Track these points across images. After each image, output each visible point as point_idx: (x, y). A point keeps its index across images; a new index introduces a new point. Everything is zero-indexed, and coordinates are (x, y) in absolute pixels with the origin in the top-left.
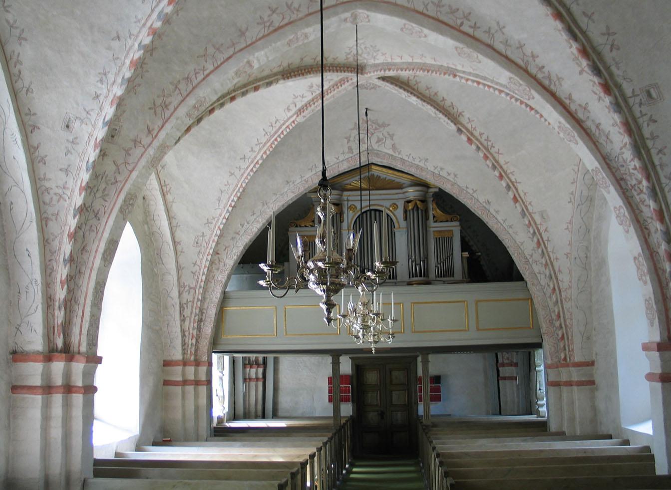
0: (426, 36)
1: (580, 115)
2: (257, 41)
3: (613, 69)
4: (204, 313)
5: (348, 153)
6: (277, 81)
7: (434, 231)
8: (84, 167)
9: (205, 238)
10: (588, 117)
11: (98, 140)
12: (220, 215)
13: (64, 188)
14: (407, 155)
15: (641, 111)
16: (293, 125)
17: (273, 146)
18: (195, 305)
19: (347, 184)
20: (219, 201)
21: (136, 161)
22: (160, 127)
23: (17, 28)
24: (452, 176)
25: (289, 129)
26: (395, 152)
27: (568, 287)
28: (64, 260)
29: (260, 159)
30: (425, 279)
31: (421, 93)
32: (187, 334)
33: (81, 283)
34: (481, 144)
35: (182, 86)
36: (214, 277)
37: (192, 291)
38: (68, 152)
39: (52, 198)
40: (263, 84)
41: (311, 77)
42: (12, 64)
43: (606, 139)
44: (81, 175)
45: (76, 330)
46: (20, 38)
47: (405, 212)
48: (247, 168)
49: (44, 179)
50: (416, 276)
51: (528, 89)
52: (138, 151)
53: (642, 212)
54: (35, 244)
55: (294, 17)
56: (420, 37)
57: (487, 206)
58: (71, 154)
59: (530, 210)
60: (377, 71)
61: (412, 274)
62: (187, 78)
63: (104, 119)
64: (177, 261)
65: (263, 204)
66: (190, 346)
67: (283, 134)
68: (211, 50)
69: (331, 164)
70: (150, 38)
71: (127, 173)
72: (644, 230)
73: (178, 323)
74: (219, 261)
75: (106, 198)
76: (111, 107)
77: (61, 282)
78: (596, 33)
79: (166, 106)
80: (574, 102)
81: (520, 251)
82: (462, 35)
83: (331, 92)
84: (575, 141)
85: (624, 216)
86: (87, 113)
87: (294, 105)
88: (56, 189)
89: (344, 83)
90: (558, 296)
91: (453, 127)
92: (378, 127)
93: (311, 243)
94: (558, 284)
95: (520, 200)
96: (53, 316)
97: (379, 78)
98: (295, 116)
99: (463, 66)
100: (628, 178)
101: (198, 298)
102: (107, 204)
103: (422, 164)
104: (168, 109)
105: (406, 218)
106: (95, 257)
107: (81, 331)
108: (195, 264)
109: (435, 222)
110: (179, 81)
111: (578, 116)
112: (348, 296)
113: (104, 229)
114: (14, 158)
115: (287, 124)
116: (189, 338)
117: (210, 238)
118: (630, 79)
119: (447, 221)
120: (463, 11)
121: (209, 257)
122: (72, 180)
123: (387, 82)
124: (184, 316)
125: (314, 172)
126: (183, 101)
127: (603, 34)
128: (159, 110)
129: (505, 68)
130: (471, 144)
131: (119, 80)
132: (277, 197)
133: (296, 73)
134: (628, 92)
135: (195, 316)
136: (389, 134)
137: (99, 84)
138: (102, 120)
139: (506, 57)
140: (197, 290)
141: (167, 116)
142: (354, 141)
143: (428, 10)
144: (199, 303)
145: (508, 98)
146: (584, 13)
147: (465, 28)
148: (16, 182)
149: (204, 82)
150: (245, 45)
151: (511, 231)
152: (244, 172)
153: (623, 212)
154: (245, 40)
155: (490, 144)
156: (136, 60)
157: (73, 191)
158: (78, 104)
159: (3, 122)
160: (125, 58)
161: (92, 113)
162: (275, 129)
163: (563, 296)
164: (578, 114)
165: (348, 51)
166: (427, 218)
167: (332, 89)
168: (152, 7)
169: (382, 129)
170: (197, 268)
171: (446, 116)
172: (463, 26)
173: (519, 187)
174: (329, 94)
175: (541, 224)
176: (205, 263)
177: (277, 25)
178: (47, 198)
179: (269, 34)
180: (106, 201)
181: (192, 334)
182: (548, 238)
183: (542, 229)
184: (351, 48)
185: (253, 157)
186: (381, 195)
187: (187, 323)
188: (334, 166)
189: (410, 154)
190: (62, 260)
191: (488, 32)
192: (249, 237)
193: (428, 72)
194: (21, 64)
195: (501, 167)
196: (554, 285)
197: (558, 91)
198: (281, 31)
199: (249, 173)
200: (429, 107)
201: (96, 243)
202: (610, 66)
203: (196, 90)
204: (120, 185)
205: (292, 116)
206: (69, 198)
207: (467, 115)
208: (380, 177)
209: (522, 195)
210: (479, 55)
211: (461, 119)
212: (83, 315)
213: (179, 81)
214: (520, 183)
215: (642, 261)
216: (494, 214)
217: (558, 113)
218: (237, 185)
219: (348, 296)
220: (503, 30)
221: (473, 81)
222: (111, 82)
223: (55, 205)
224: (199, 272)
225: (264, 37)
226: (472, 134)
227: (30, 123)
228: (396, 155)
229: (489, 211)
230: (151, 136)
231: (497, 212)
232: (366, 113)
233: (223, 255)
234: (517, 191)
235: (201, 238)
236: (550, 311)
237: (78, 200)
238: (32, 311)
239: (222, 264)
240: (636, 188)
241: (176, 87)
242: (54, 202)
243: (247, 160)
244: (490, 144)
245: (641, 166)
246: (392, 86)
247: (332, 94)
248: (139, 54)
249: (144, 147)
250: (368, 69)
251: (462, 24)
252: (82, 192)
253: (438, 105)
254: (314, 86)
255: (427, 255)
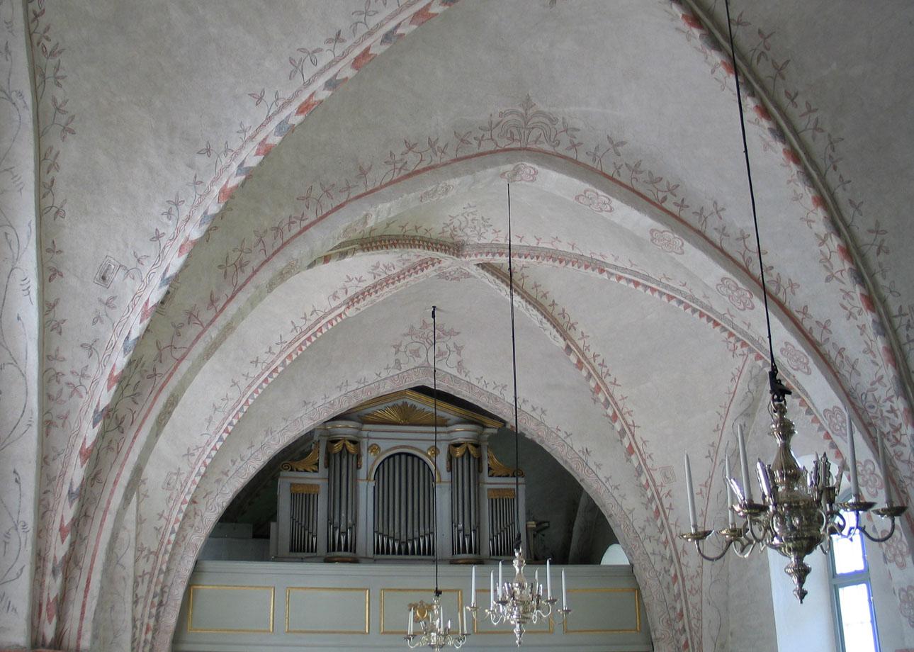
0: (611, 210)
1: (817, 336)
2: (382, 187)
3: (879, 277)
4: (165, 592)
5: (393, 368)
6: (355, 251)
7: (489, 490)
8: (120, 345)
9: (181, 477)
10: (828, 339)
11: (150, 305)
12: (208, 443)
13: (83, 376)
14: (477, 379)
15: (908, 336)
16: (339, 320)
17: (304, 348)
18: (155, 580)
19: (368, 414)
20: (210, 422)
21: (188, 346)
22: (229, 297)
23: (64, 112)
24: (539, 411)
25: (332, 325)
26: (460, 373)
27: (696, 574)
28: (70, 493)
29: (279, 365)
30: (476, 556)
31: (526, 292)
32: (138, 624)
33: (87, 534)
34: (594, 370)
35: (268, 239)
36: (185, 538)
37: (152, 557)
38: (97, 319)
39: (62, 390)
40: (336, 253)
41: (374, 254)
42: (45, 165)
43: (850, 370)
44: (113, 359)
45: (74, 611)
46: (67, 130)
47: (450, 458)
48: (259, 377)
49: (56, 358)
50: (464, 552)
51: (748, 295)
52: (192, 331)
53: (897, 469)
54: (30, 462)
55: (437, 160)
56: (602, 210)
57: (584, 458)
58: (102, 322)
59: (649, 466)
60: (481, 254)
61: (457, 549)
62: (278, 228)
63: (164, 274)
64: (138, 510)
65: (267, 433)
66: (142, 644)
67: (321, 332)
68: (317, 191)
69: (370, 383)
70: (260, 158)
71: (172, 363)
72: (901, 494)
73: (129, 606)
74: (196, 513)
75: (137, 399)
76: (179, 256)
77: (61, 529)
78: (861, 226)
79: (240, 266)
80: (810, 317)
81: (628, 523)
82: (664, 214)
83: (404, 278)
84: (806, 370)
85: (873, 473)
86: (138, 260)
87: (344, 291)
88: (71, 376)
89: (427, 268)
90: (681, 587)
91: (561, 343)
92: (442, 335)
93: (312, 496)
94: (681, 569)
95: (637, 451)
96: (41, 586)
97: (478, 265)
98: (343, 308)
99: (616, 259)
100: (879, 422)
101: (160, 569)
102: (137, 408)
103: (496, 393)
104: (243, 272)
105: (450, 469)
106: (112, 492)
107: (83, 613)
108: (161, 516)
109: (490, 476)
110: (266, 232)
111: (813, 337)
112: (468, 576)
113: (131, 448)
114: (19, 318)
115: (330, 317)
116: (141, 630)
117: (188, 477)
118: (898, 293)
119: (508, 476)
120: (668, 183)
121: (184, 507)
122: (96, 365)
123: (488, 271)
124: (137, 595)
125: (343, 392)
126: (266, 261)
127: (870, 231)
128: (231, 270)
129: (718, 262)
130: (581, 370)
131: (198, 216)
132: (288, 423)
133: (378, 244)
134: (894, 310)
135: (154, 597)
136: (455, 346)
137: (165, 217)
138: (161, 274)
139: (722, 250)
140: (160, 556)
141: (241, 281)
142: (405, 352)
143: (619, 176)
144: (162, 576)
145: (682, 307)
146: (851, 202)
147: (668, 205)
148: (13, 358)
149: (301, 237)
150: (364, 191)
151: (616, 493)
152: (253, 383)
153: (872, 468)
154: (366, 184)
155: (605, 370)
156: (231, 189)
157: (95, 382)
158: (126, 245)
159: (13, 257)
160: (213, 182)
161: (145, 262)
162: (309, 324)
163: (688, 587)
164: (813, 334)
165: (448, 222)
166: (480, 470)
167: (407, 273)
168: (269, 112)
169: (447, 338)
170: (163, 522)
171: (554, 327)
172: (666, 202)
173: (637, 432)
174: (402, 280)
175: (662, 486)
176: (176, 515)
177: (411, 168)
178: (54, 390)
179: (399, 180)
180: (136, 403)
181: (148, 625)
182: (671, 505)
183: (663, 492)
184: (453, 218)
185: (269, 361)
186: (421, 432)
187: (140, 607)
188: (373, 386)
189: (482, 377)
190: (65, 492)
191: (700, 213)
192: (243, 481)
193: (561, 262)
194: (57, 169)
195: (616, 403)
196: (676, 571)
197: (788, 301)
198: (416, 177)
199: (261, 384)
200: (535, 312)
201: (116, 470)
202: (874, 274)
203: (287, 249)
204: (160, 381)
205: (338, 307)
206: (87, 393)
207: (580, 328)
208: (415, 407)
209: (640, 444)
210: (686, 243)
211: (572, 333)
212: (88, 586)
213: (266, 232)
214: (639, 427)
215: (899, 536)
216: (594, 468)
217: (788, 330)
218: (239, 401)
219: (468, 576)
220: (721, 213)
221: (629, 281)
222: (183, 217)
223: (65, 402)
224: (166, 530)
225: (391, 183)
226: (583, 355)
227: (51, 265)
228: (462, 377)
229: (587, 464)
230: (214, 308)
231: (598, 466)
232: (433, 313)
233: (201, 507)
234: (634, 439)
235: (175, 477)
236: (667, 608)
237: (104, 396)
238: (12, 575)
239: (198, 518)
240: (891, 437)
241: (261, 240)
242: (64, 397)
243: (259, 365)
244: (605, 370)
245: (907, 407)
246: (492, 278)
247: (406, 280)
248: (235, 181)
249: (202, 325)
250: (467, 250)
251: (665, 199)
252: (113, 385)
253: (545, 310)
254: (381, 266)
255: (479, 523)
